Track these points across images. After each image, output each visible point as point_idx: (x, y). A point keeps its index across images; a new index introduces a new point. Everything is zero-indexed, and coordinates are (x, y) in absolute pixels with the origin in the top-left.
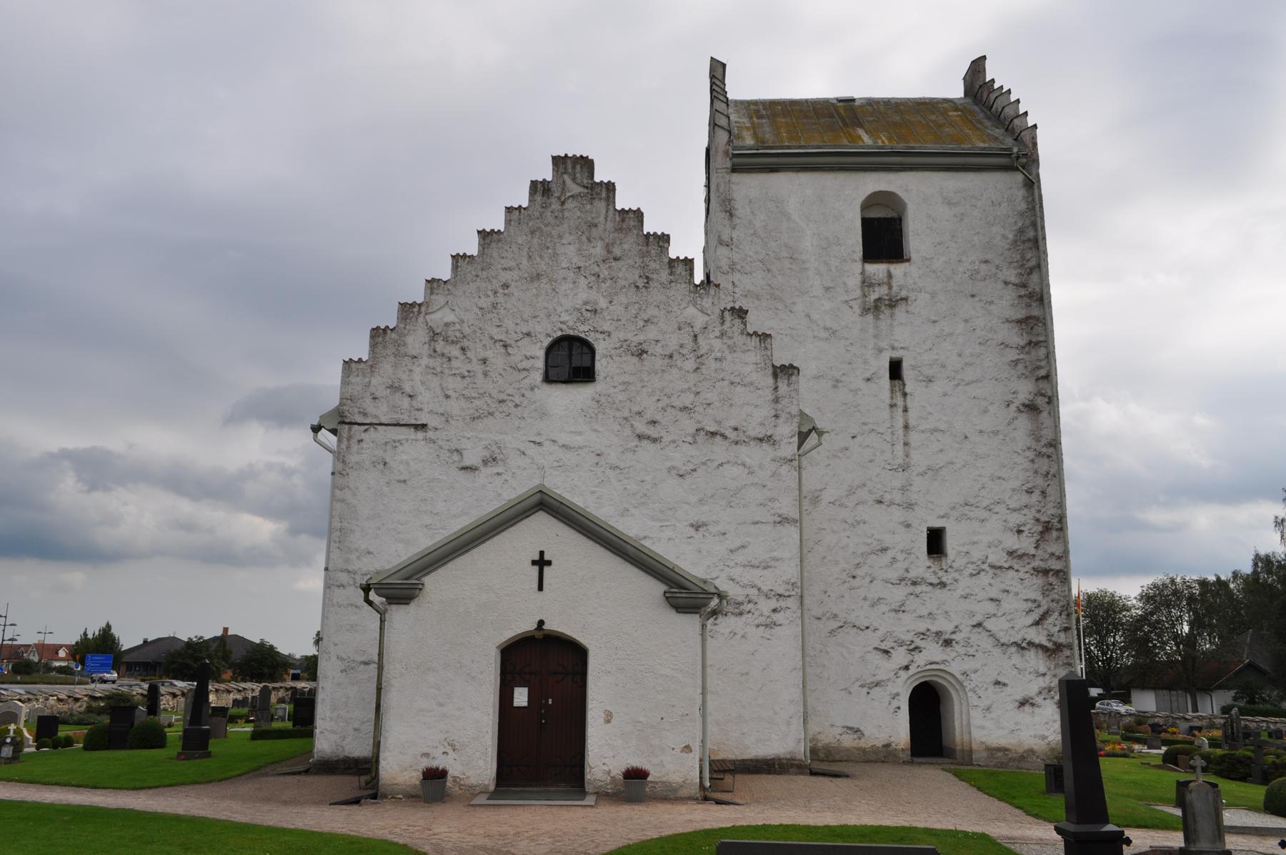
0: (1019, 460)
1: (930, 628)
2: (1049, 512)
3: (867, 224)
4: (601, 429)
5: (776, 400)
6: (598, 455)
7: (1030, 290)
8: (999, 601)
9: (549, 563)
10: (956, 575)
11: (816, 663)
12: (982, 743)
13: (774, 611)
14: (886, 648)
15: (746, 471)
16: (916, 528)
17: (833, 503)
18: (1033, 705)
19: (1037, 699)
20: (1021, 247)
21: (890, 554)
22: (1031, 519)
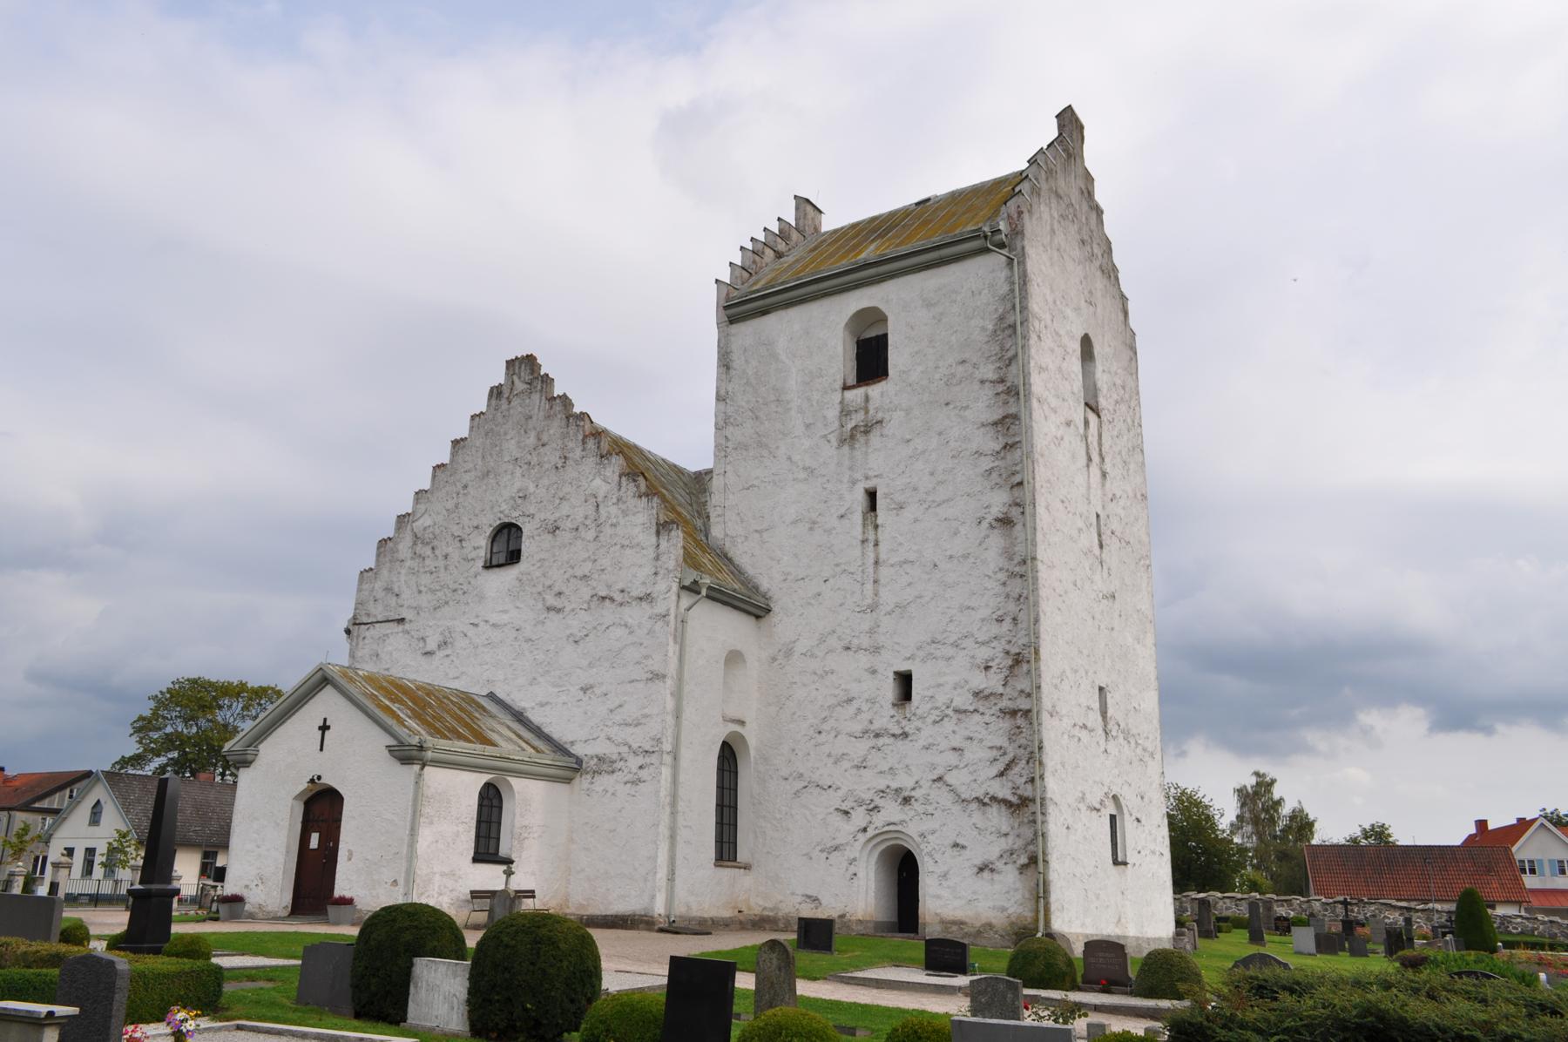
0: (990, 584)
1: (890, 785)
2: (1020, 642)
4: (522, 606)
5: (657, 558)
6: (517, 630)
7: (1009, 384)
8: (962, 750)
10: (919, 724)
11: (782, 826)
12: (936, 914)
13: (641, 767)
14: (846, 809)
15: (627, 631)
16: (882, 674)
17: (805, 655)
18: (992, 870)
19: (997, 864)
20: (1000, 337)
21: (855, 704)
22: (1000, 652)
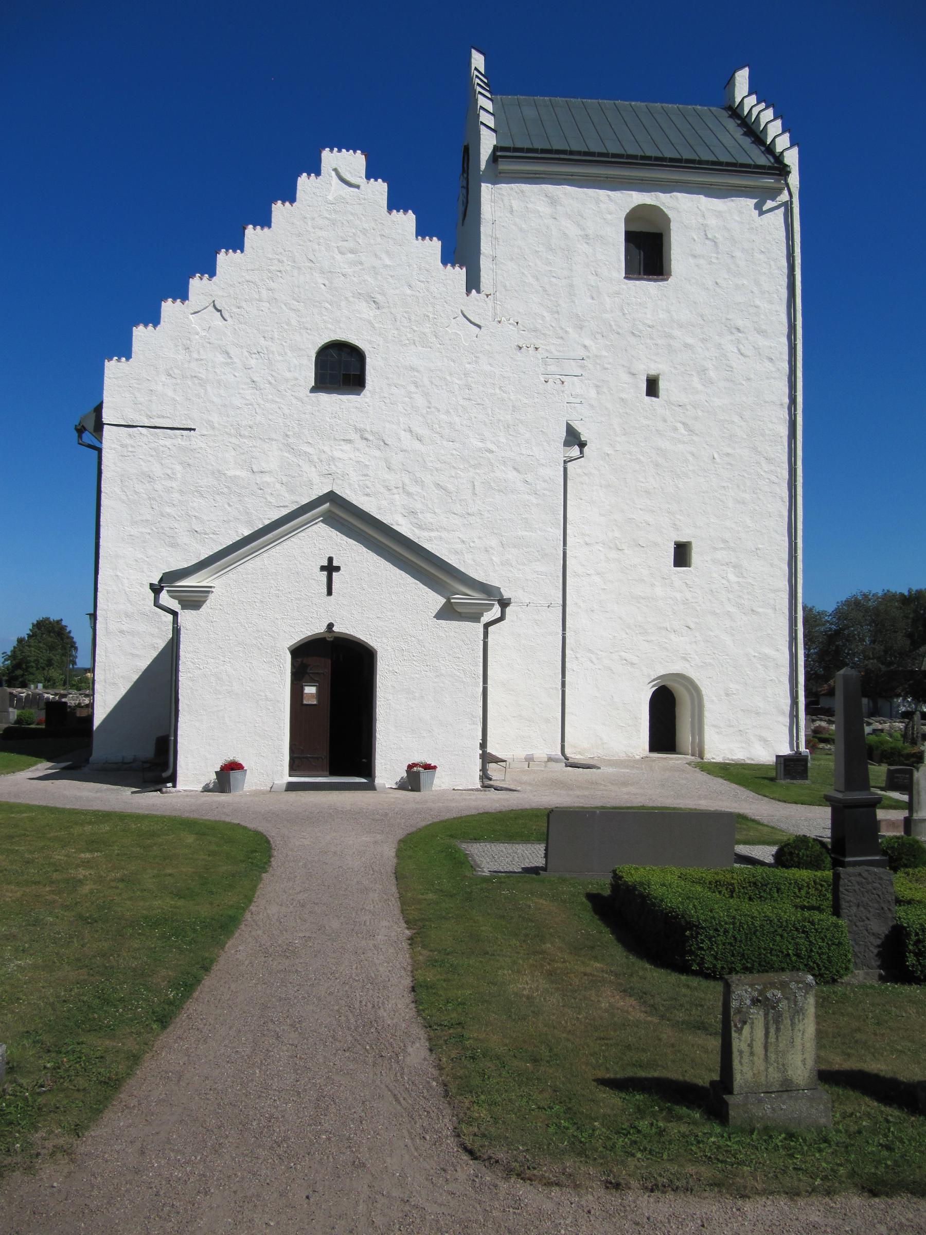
3: (631, 237)
9: (338, 569)
